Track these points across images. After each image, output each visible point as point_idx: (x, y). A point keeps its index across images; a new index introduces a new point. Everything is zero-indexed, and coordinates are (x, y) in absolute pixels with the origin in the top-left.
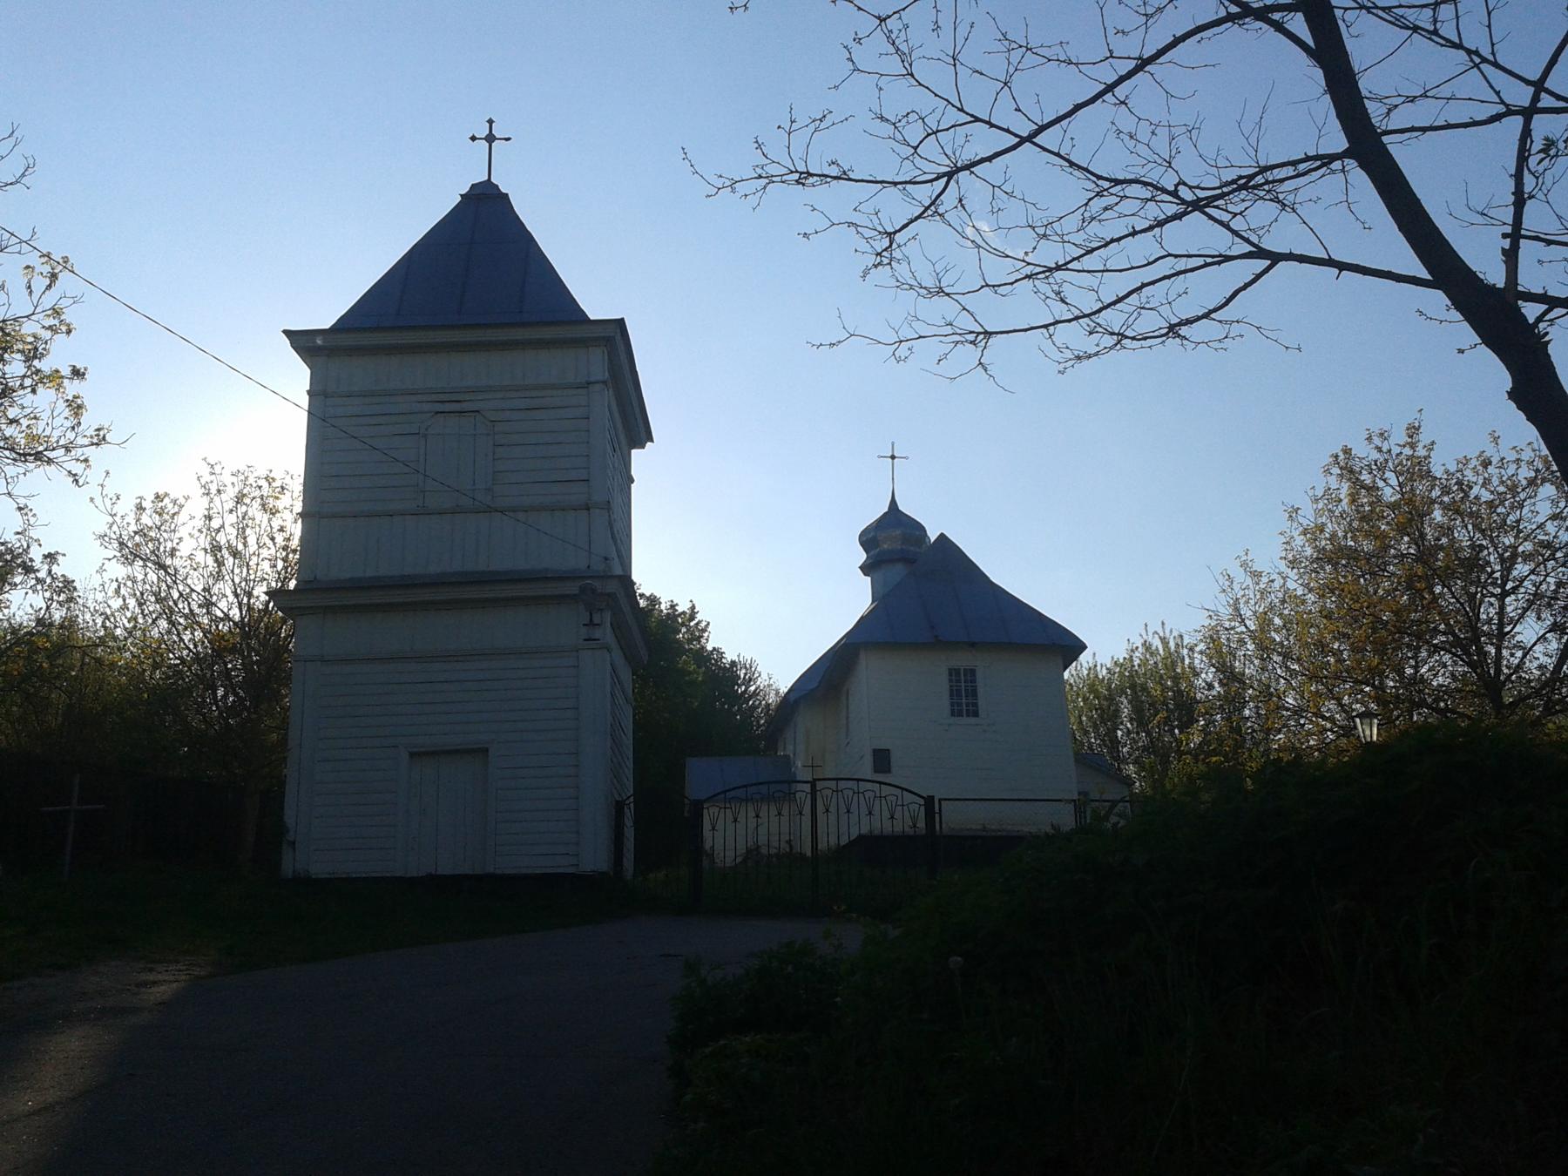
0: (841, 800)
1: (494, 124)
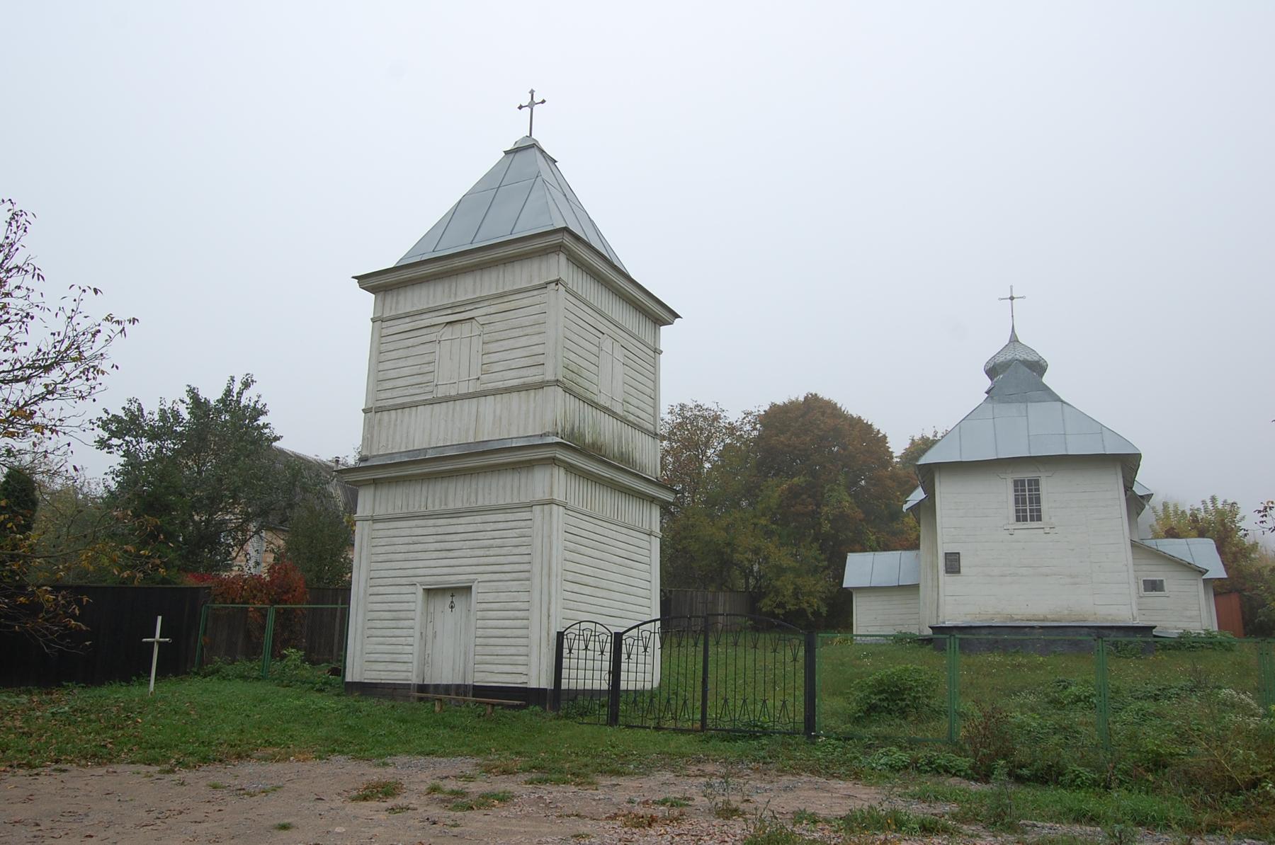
1: (534, 94)
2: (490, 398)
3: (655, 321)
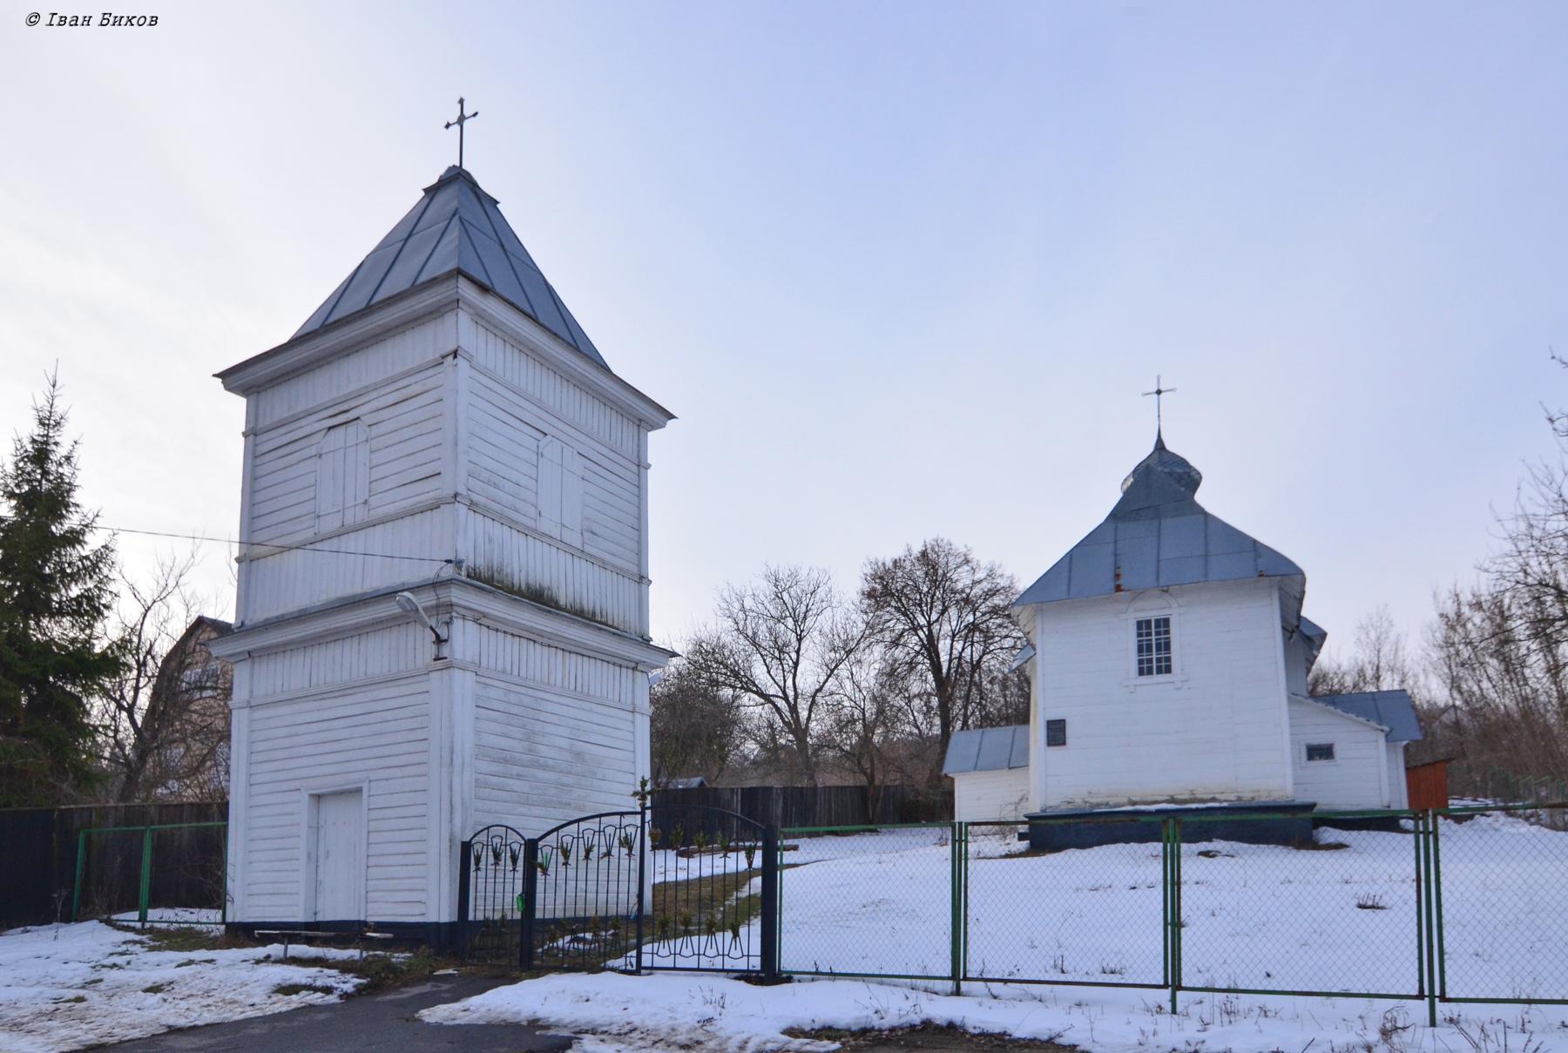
0: (602, 837)
2: (379, 528)
3: (637, 422)
